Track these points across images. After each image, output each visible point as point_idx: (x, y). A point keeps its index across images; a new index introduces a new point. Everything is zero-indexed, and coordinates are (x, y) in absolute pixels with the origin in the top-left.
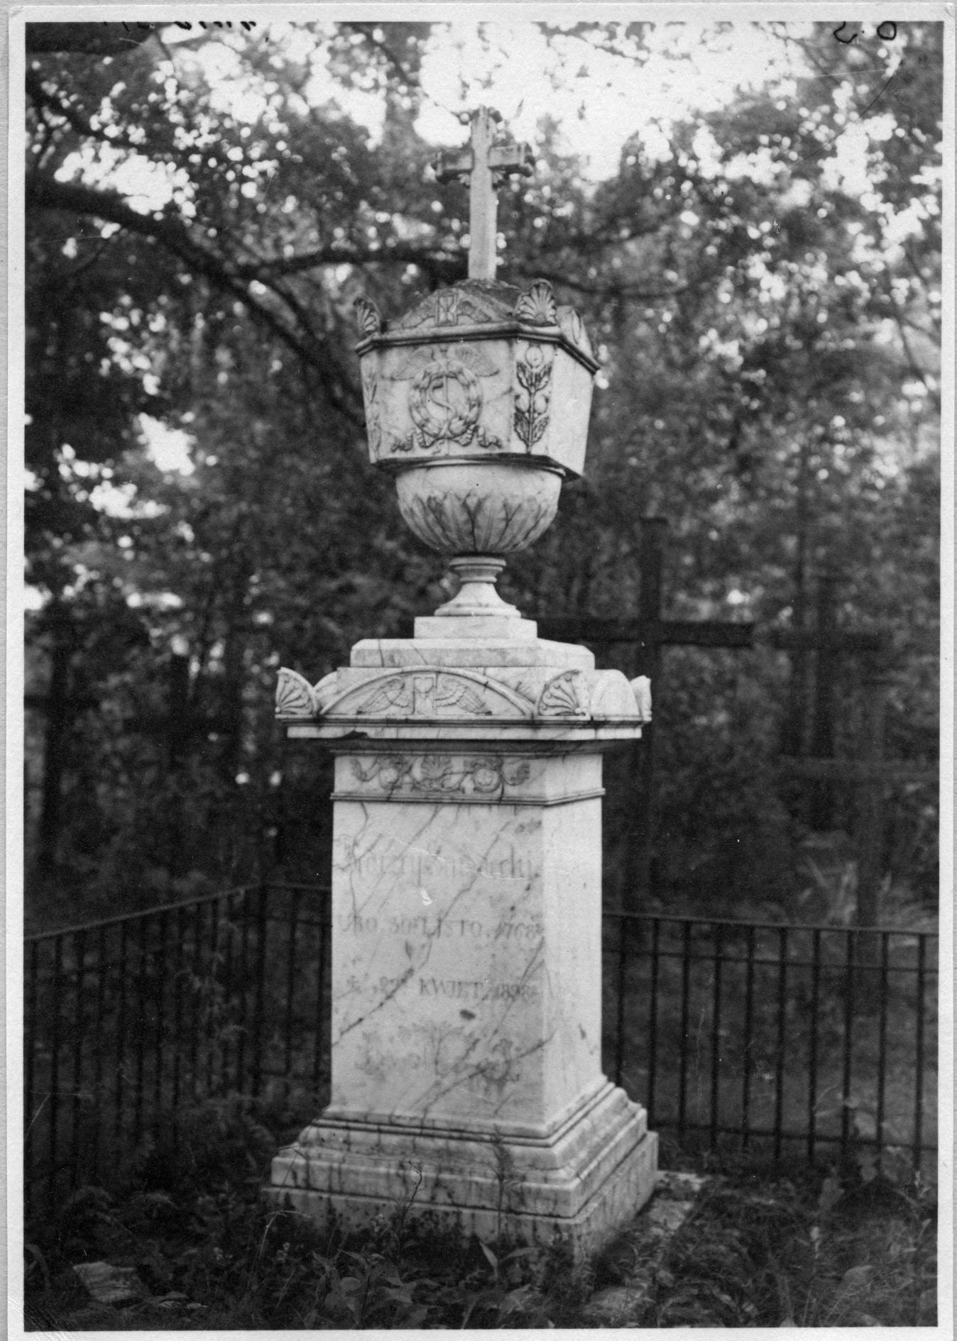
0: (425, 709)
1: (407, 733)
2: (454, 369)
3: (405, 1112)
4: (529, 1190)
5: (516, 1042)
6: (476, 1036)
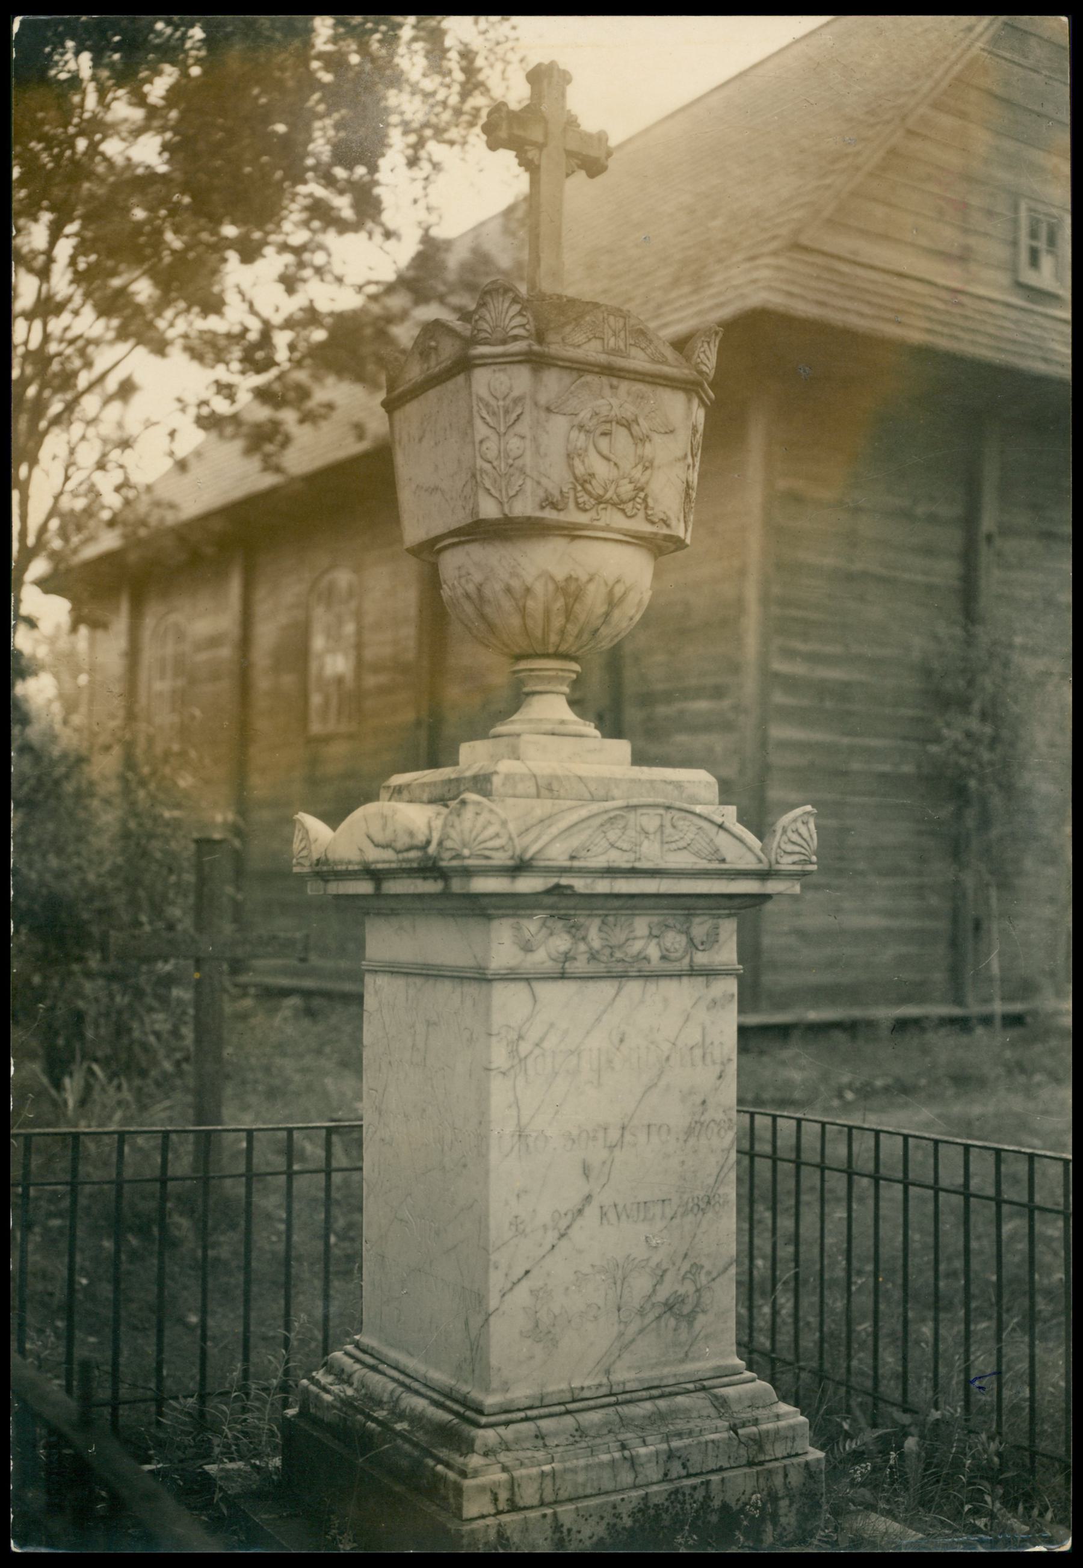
0: (652, 854)
1: (624, 886)
2: (629, 415)
3: (586, 1380)
4: (768, 1432)
5: (707, 1265)
6: (664, 1267)
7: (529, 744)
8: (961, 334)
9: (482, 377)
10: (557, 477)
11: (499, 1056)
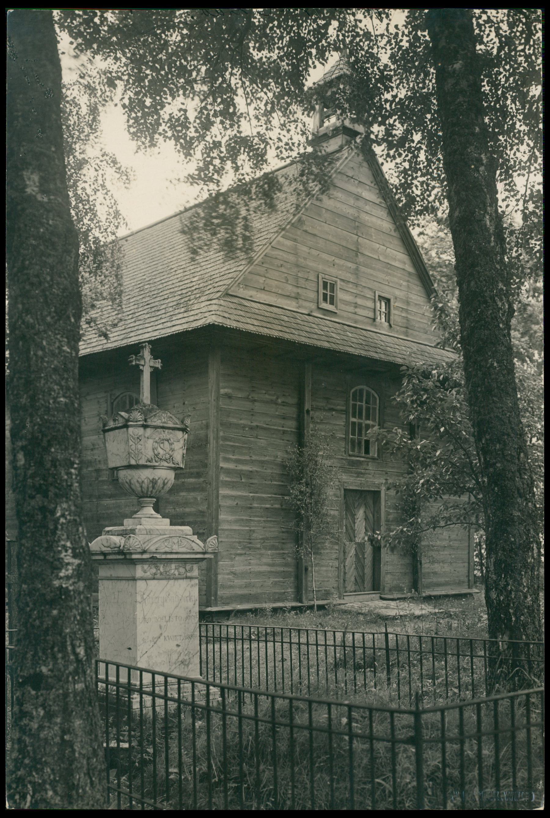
0: (176, 548)
1: (169, 556)
7: (143, 521)
8: (294, 331)
9: (131, 430)
10: (150, 454)
11: (139, 598)
